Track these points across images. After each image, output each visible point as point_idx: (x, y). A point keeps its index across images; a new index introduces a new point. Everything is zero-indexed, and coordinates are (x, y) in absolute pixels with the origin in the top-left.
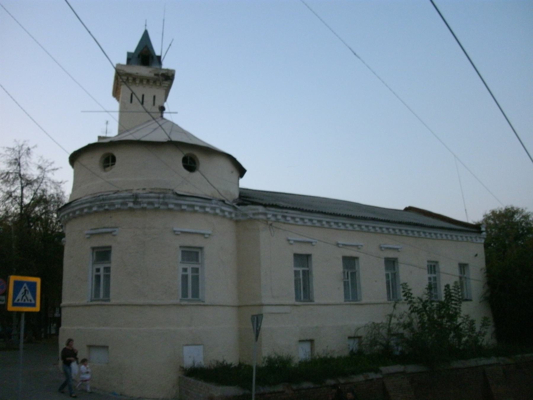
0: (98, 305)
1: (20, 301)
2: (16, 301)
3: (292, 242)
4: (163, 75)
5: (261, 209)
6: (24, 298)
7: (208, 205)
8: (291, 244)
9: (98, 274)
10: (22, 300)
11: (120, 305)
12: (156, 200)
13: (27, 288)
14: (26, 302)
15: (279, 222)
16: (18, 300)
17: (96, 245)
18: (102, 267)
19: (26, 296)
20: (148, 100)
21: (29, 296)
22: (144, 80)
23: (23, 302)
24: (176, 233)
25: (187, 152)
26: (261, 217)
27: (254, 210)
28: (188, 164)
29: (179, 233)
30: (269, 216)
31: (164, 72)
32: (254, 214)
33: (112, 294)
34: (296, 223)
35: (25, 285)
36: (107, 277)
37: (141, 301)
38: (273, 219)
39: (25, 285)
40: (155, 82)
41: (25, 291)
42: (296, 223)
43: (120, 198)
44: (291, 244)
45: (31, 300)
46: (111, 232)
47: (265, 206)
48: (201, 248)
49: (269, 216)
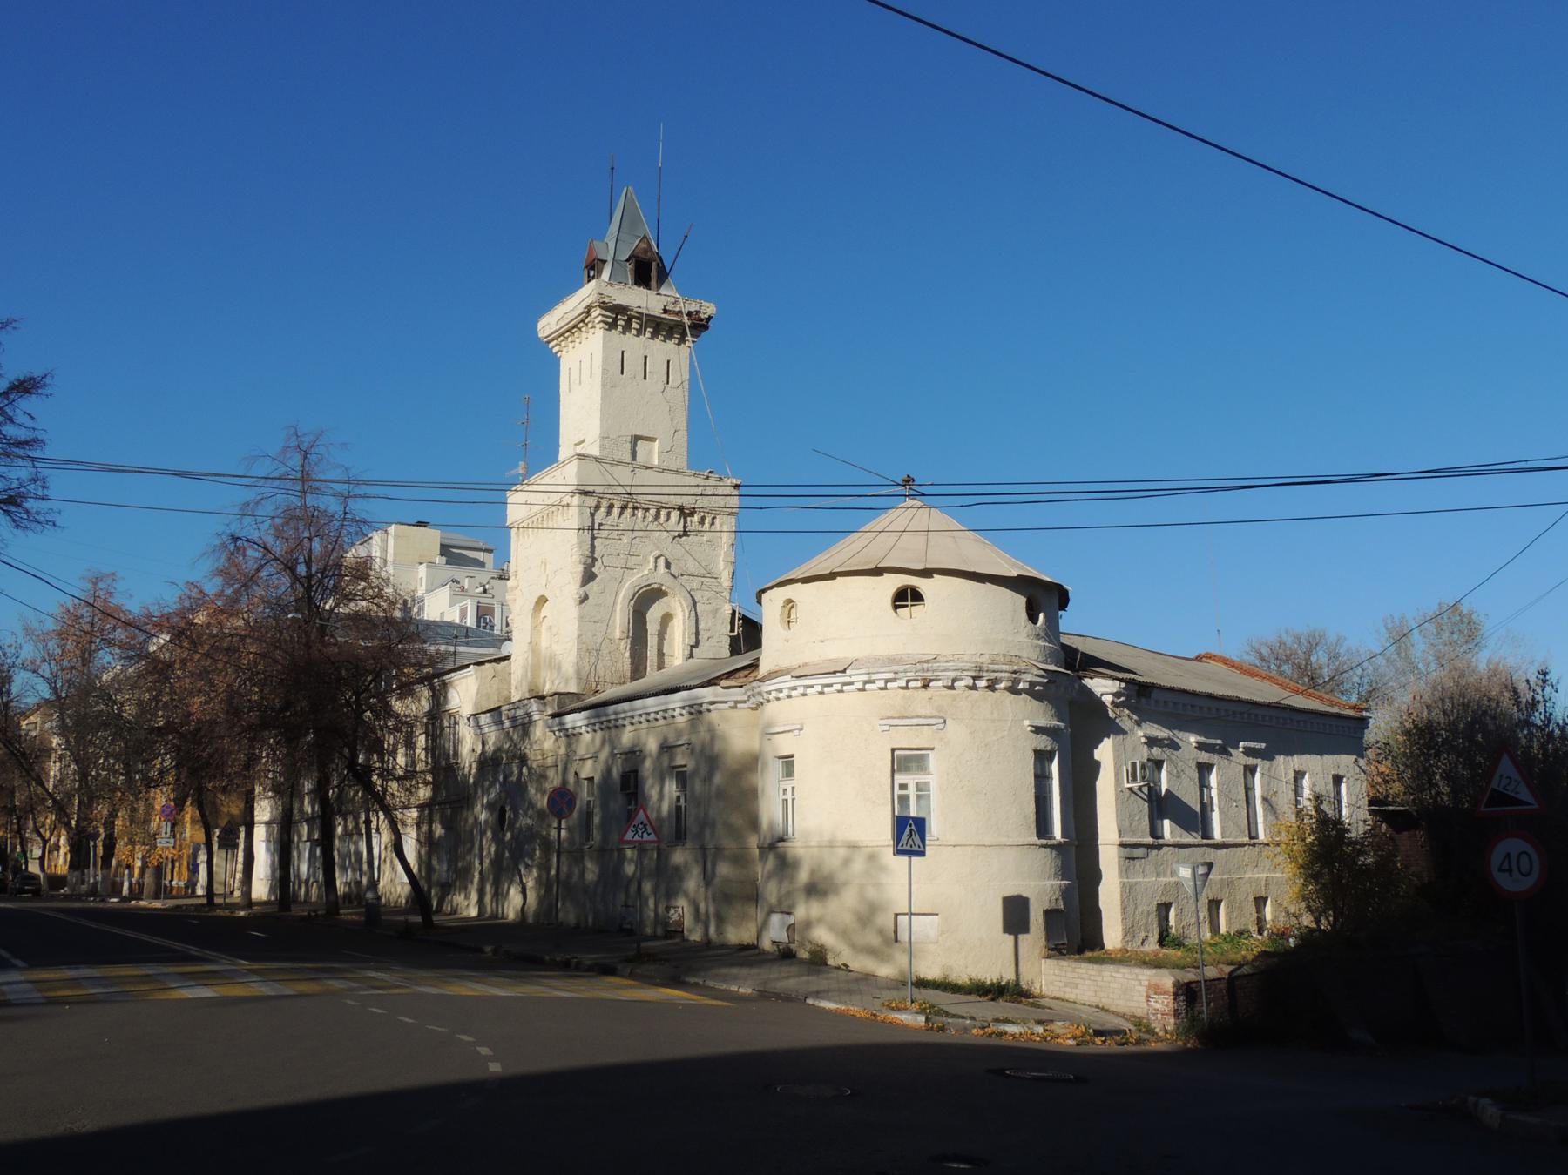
1: (905, 848)
2: (900, 848)
6: (910, 841)
9: (785, 797)
12: (1006, 675)
13: (913, 827)
16: (902, 846)
18: (910, 780)
21: (917, 838)
23: (908, 848)
25: (893, 583)
35: (911, 822)
39: (911, 822)
41: (911, 830)
45: (919, 847)
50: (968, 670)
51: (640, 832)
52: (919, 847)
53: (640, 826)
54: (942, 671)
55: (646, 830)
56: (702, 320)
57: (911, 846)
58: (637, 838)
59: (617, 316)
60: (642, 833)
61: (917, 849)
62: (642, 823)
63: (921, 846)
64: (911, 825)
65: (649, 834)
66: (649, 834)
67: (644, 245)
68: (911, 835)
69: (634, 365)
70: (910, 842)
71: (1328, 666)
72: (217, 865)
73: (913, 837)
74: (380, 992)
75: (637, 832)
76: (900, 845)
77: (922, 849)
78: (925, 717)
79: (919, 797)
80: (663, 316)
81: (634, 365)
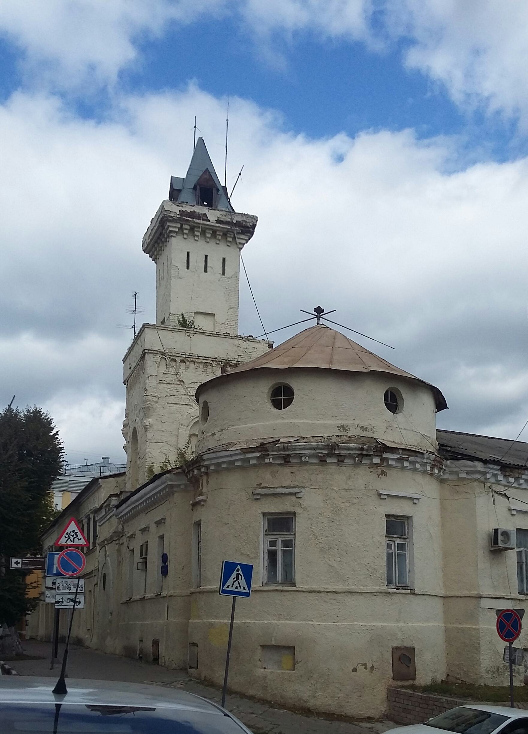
0: (272, 591)
1: (230, 589)
2: (225, 588)
3: (514, 512)
4: (238, 224)
5: (480, 466)
7: (418, 460)
8: (513, 515)
10: (232, 587)
11: (310, 592)
12: (90, 512)
13: (240, 572)
14: (239, 590)
15: (499, 484)
17: (272, 509)
19: (239, 582)
20: (215, 263)
21: (243, 582)
22: (207, 231)
23: (234, 589)
24: (382, 497)
26: (477, 476)
27: (471, 467)
28: (389, 402)
29: (385, 497)
30: (488, 476)
31: (240, 219)
32: (468, 473)
33: (298, 577)
34: (520, 487)
35: (239, 567)
36: (289, 555)
37: (338, 587)
38: (493, 480)
39: (239, 567)
40: (225, 235)
41: (238, 575)
42: (520, 487)
43: (311, 449)
44: (513, 515)
45: (244, 589)
46: (295, 494)
47: (485, 462)
48: (408, 518)
49: (488, 476)
50: (320, 449)
51: (72, 538)
52: (244, 589)
53: (72, 534)
54: (300, 449)
55: (77, 536)
56: (248, 227)
57: (237, 588)
58: (69, 542)
59: (182, 226)
60: (74, 538)
61: (242, 590)
62: (73, 531)
63: (246, 588)
64: (238, 570)
65: (79, 540)
66: (79, 540)
67: (207, 177)
68: (238, 579)
69: (197, 261)
70: (236, 584)
71: (245, 540)
72: (205, 380)
73: (240, 580)
74: (40, 617)
75: (70, 538)
76: (226, 585)
77: (247, 591)
78: (287, 487)
79: (284, 552)
80: (217, 225)
81: (197, 261)
